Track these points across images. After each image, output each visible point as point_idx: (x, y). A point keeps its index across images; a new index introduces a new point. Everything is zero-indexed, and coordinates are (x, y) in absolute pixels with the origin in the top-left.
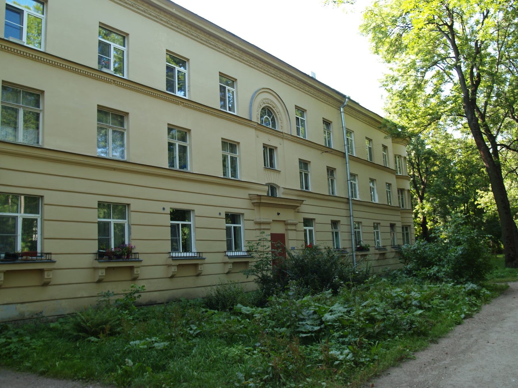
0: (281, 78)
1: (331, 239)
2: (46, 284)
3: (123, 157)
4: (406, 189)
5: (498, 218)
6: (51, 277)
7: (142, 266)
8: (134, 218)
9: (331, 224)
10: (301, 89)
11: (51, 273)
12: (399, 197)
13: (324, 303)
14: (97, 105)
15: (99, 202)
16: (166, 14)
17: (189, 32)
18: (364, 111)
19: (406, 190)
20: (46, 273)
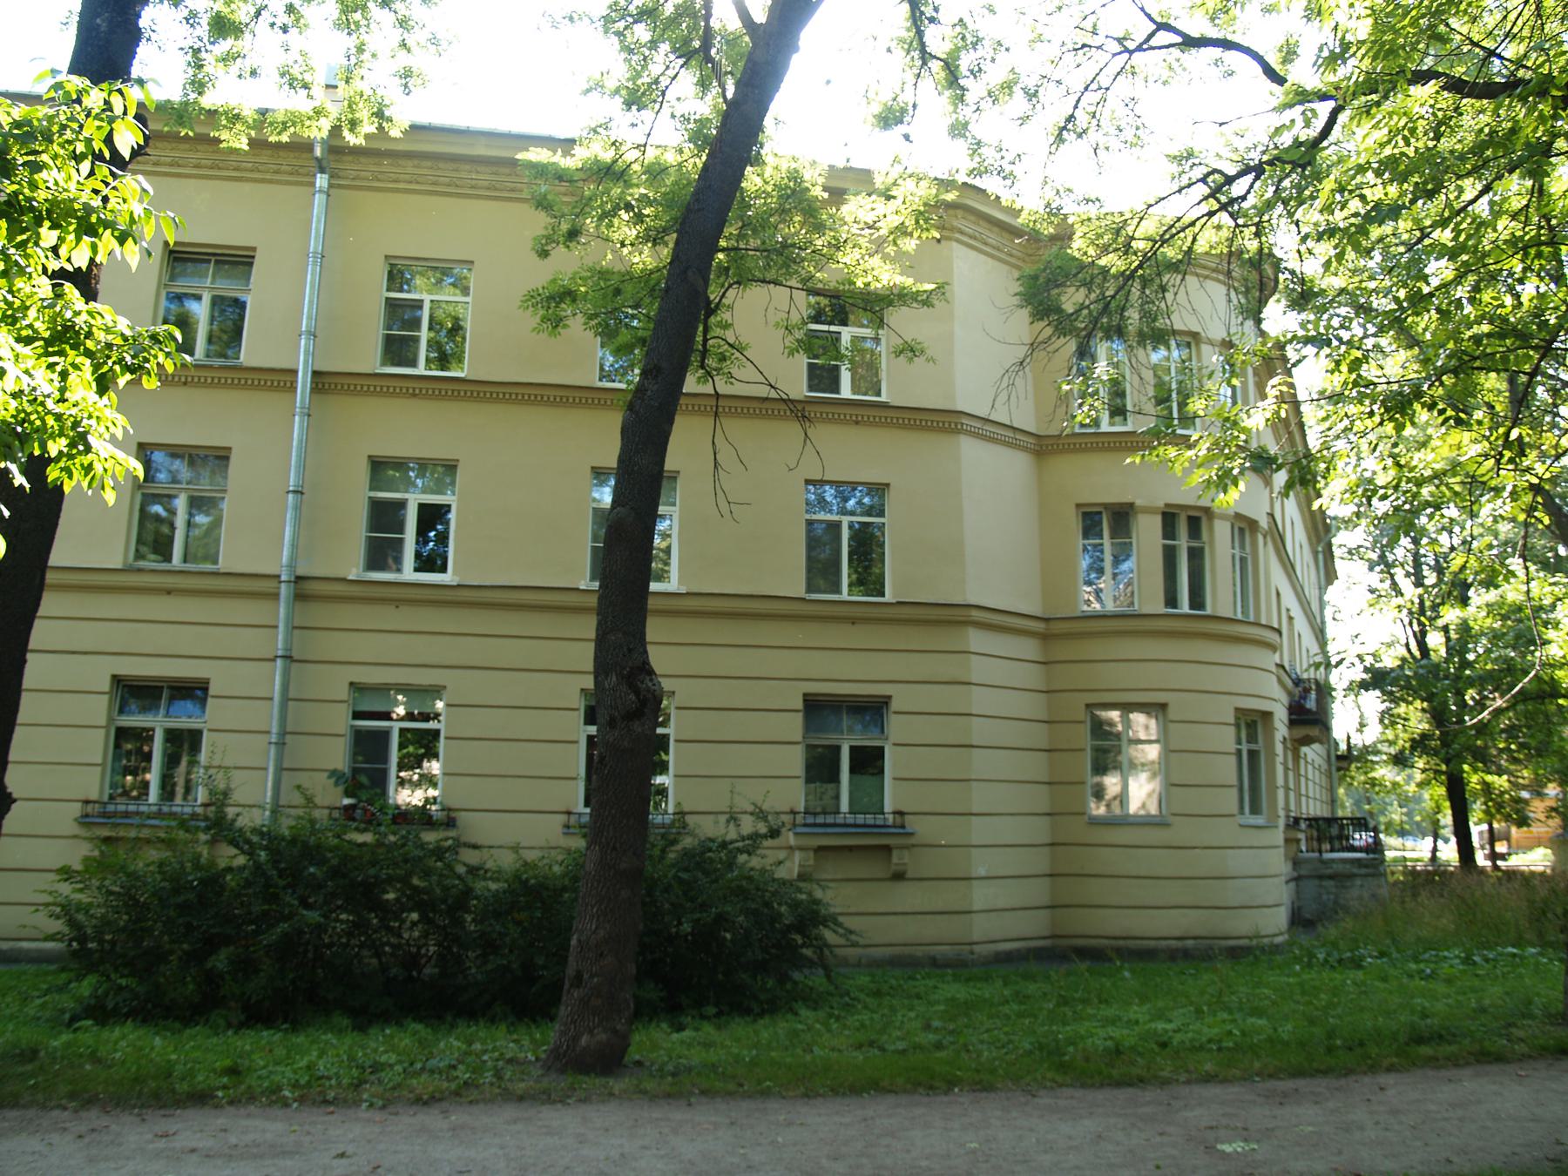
0: (975, 238)
1: (1234, 780)
2: (899, 876)
3: (1248, 617)
4: (1138, 502)
5: (417, 477)
6: (906, 861)
7: (913, 846)
8: (897, 727)
9: (1237, 726)
10: (401, 186)
11: (906, 853)
12: (1170, 556)
13: (1427, 1017)
14: (589, 470)
15: (805, 695)
16: (416, 162)
17: (419, 179)
18: (481, 150)
19: (1224, 517)
20: (895, 853)
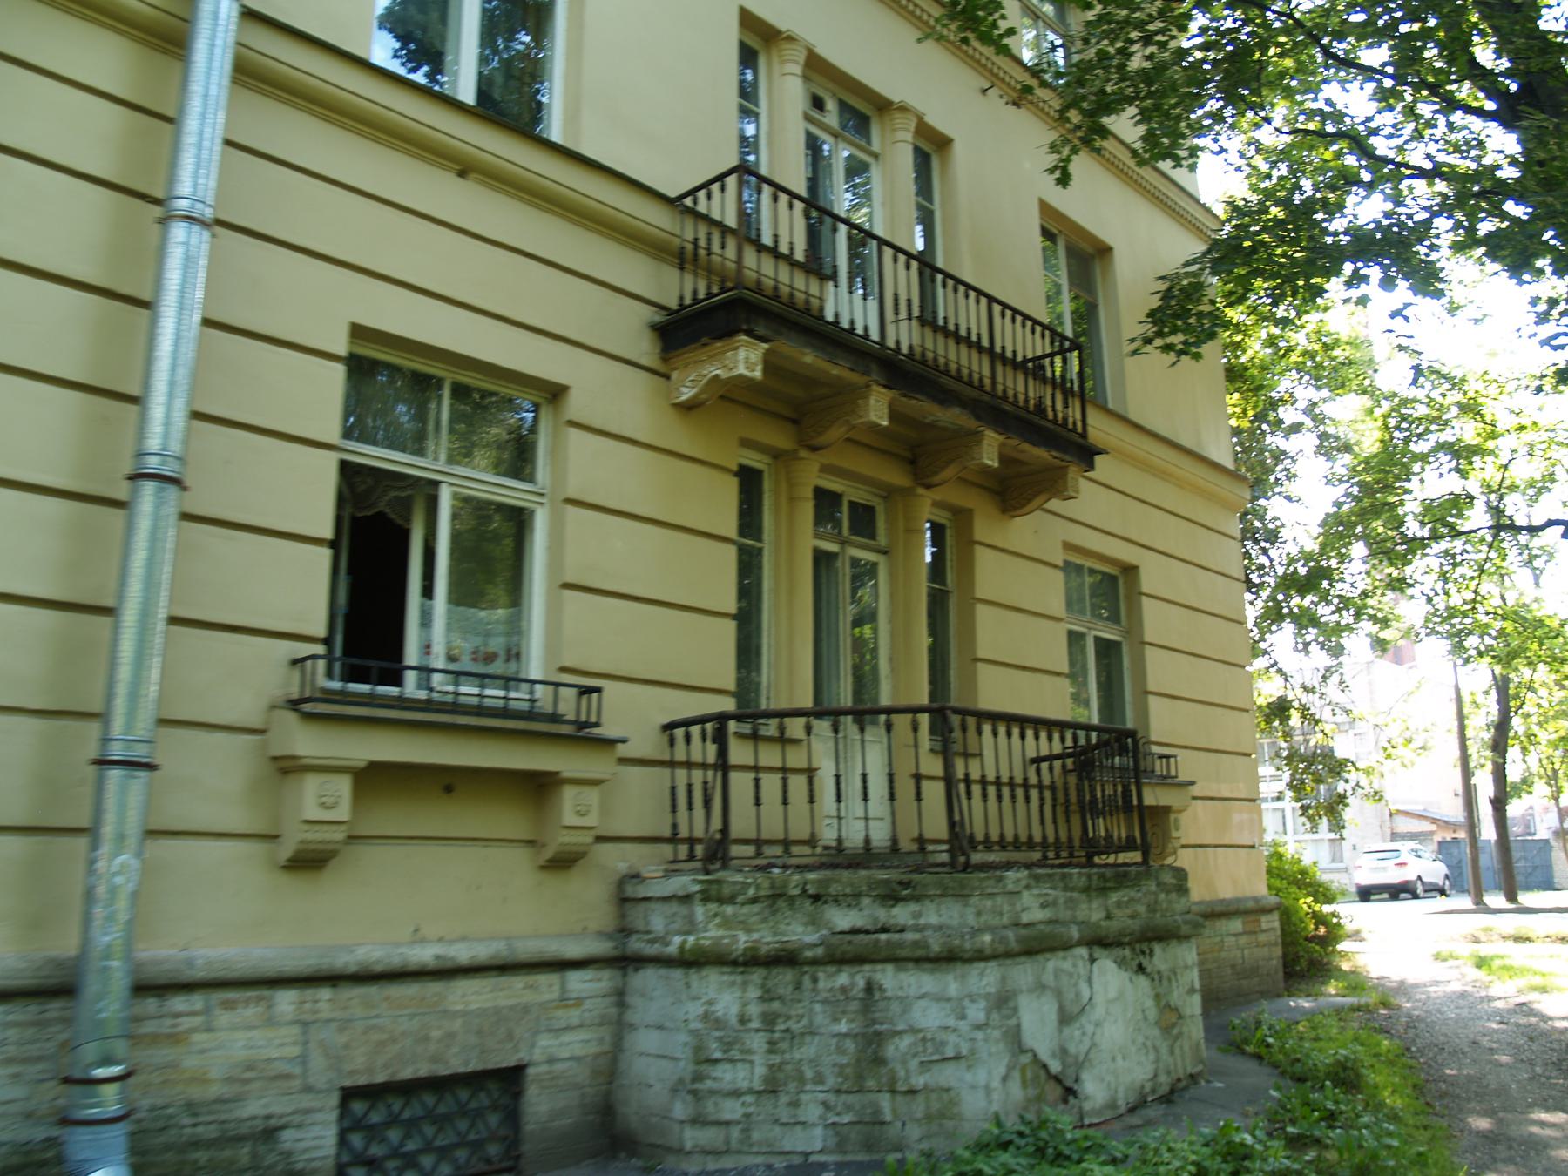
20: (569, 794)
